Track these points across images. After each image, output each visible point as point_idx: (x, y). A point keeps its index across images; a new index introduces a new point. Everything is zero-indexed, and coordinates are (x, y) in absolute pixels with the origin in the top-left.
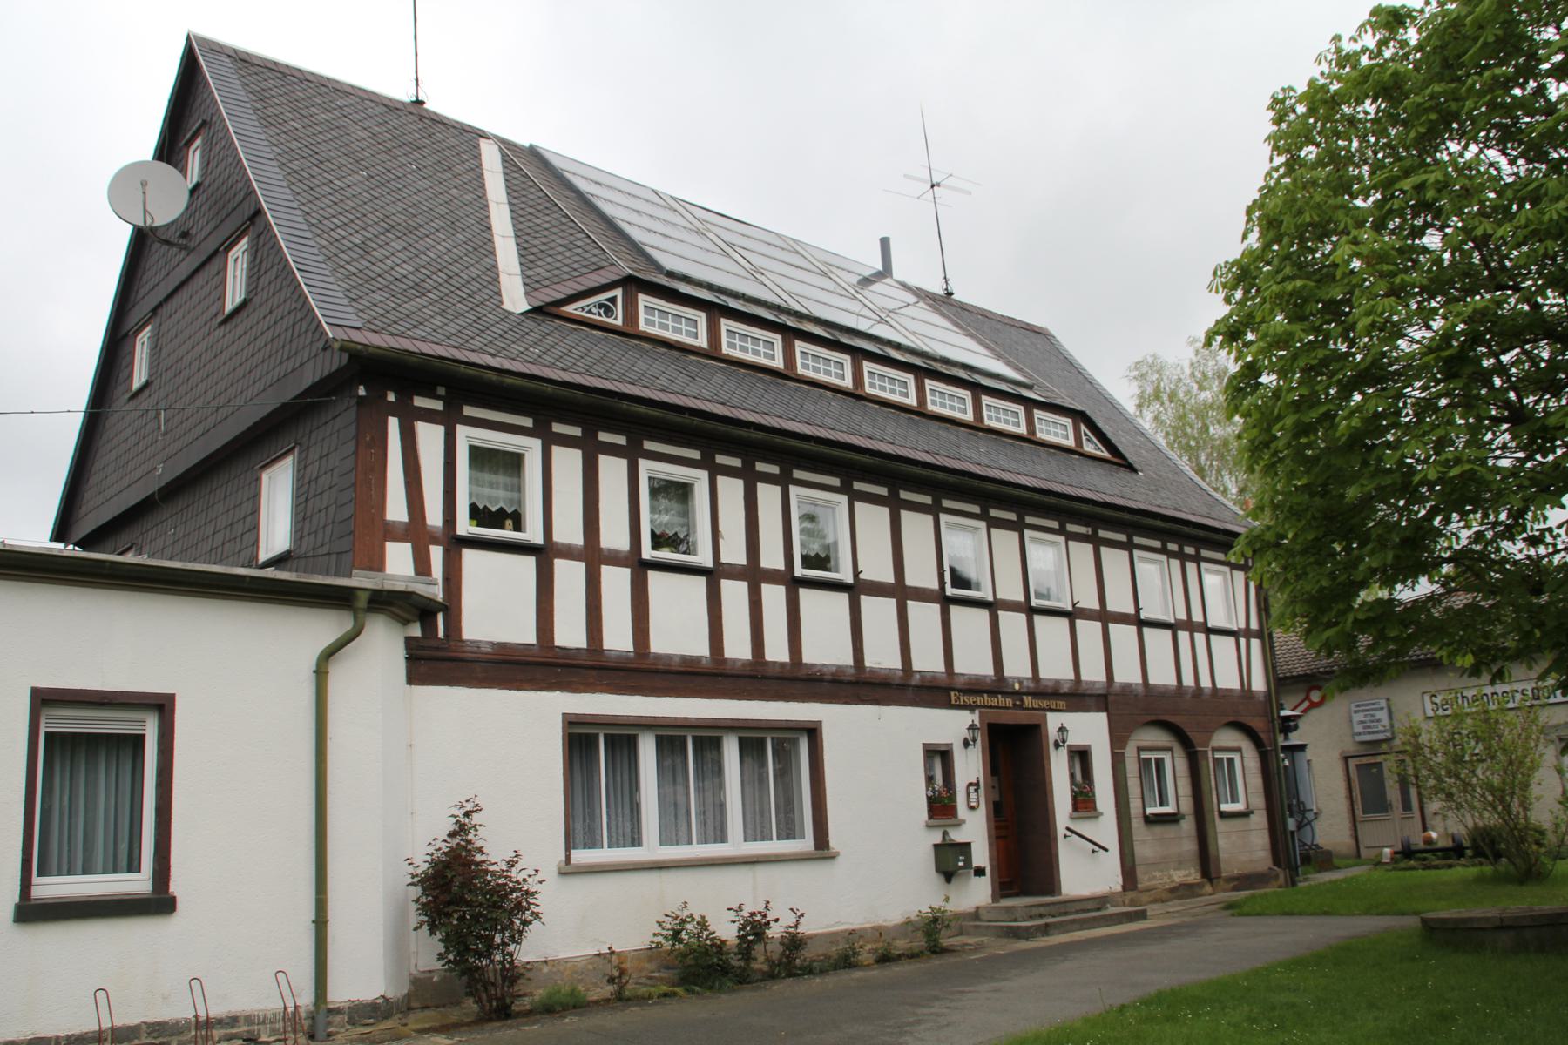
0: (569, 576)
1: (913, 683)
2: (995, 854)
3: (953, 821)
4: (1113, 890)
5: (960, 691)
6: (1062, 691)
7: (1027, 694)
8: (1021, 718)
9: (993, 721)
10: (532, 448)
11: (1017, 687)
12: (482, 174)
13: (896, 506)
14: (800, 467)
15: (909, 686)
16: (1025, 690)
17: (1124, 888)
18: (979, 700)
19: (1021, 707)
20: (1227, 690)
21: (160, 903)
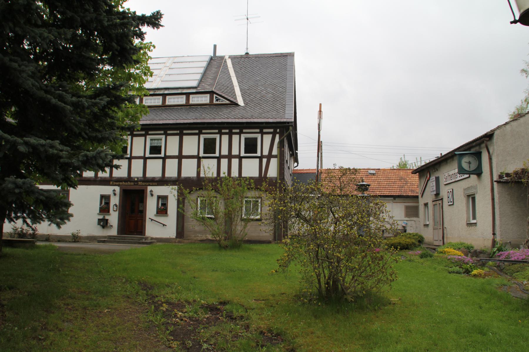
0: (224, 162)
1: (98, 180)
3: (108, 214)
4: (171, 237)
5: (114, 181)
6: (155, 180)
7: (140, 181)
8: (137, 188)
9: (125, 189)
11: (136, 179)
12: (231, 79)
13: (181, 136)
14: (204, 130)
15: (97, 181)
16: (139, 180)
17: (177, 237)
18: (121, 183)
19: (137, 185)
20: (169, 177)
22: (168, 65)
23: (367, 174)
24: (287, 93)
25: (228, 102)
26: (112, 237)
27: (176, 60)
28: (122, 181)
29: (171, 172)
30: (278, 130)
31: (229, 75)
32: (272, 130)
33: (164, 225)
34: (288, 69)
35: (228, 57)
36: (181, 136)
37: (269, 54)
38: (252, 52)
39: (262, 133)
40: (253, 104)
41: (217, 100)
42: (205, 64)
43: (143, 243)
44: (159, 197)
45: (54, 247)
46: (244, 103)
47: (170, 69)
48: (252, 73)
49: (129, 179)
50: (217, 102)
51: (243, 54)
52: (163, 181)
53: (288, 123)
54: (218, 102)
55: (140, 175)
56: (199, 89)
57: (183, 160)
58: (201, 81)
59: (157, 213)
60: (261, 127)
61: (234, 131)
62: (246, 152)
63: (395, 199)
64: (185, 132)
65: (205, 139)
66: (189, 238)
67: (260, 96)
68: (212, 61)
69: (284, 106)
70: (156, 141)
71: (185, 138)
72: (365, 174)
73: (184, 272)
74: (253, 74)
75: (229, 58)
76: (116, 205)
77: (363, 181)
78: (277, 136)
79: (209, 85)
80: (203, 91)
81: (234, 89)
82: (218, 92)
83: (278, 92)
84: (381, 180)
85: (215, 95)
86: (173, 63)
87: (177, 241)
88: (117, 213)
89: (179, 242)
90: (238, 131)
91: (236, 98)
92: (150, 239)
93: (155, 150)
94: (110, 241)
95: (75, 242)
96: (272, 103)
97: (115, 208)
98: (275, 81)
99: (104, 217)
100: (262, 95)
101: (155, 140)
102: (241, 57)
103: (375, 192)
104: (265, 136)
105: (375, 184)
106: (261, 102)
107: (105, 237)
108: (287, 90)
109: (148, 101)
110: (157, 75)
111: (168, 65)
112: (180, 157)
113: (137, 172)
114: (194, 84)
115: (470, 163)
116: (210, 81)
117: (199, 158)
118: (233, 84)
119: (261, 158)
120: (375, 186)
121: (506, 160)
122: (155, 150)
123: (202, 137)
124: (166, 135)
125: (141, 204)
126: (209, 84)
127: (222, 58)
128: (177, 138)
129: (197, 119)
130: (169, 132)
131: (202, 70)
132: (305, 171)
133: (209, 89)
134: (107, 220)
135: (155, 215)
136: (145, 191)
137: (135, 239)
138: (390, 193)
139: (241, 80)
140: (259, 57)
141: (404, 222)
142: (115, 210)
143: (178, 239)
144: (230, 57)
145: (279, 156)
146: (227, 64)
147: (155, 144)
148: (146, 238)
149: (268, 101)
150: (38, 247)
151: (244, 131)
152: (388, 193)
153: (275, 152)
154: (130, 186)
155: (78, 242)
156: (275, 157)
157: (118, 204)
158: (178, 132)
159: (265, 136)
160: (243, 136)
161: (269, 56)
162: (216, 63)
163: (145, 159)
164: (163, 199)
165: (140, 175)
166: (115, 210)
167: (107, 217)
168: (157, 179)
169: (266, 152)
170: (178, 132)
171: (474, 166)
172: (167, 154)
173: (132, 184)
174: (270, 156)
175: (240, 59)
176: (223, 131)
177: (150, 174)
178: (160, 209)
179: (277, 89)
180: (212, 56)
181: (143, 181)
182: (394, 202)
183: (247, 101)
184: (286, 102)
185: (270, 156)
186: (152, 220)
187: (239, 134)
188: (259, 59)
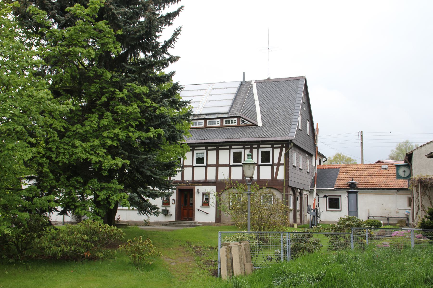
2: (177, 212)
4: (212, 222)
7: (190, 183)
8: (188, 187)
10: (271, 150)
11: (187, 182)
13: (217, 150)
17: (216, 222)
19: (188, 185)
21: (341, 211)
22: (208, 91)
23: (380, 169)
24: (294, 115)
25: (250, 124)
26: (171, 222)
27: (215, 86)
28: (177, 183)
29: (211, 176)
30: (284, 145)
31: (254, 99)
32: (280, 145)
33: (207, 213)
34: (298, 93)
35: (254, 81)
36: (217, 150)
37: (286, 78)
38: (272, 77)
39: (273, 148)
40: (268, 125)
41: (243, 122)
42: (235, 90)
43: (193, 226)
44: (203, 194)
45: (138, 228)
46: (262, 124)
47: (209, 95)
48: (271, 96)
49: (182, 181)
50: (243, 124)
51: (266, 78)
52: (206, 183)
53: (291, 140)
54: (244, 124)
55: (190, 178)
56: (230, 114)
57: (219, 168)
58: (232, 107)
59: (202, 205)
60: (273, 143)
61: (254, 146)
62: (262, 161)
63: (399, 191)
64: (220, 147)
65: (234, 153)
66: (224, 222)
67: (274, 118)
68: (241, 87)
69: (290, 126)
70: (200, 154)
71: (220, 151)
72: (378, 169)
73: (209, 238)
74: (272, 97)
75: (255, 83)
76: (174, 200)
77: (352, 180)
78: (284, 149)
79: (237, 110)
80: (232, 116)
81: (256, 112)
82: (243, 117)
83: (288, 114)
84: (391, 175)
85: (241, 119)
86: (213, 89)
87: (216, 225)
88: (174, 206)
89: (217, 225)
90: (256, 146)
91: (256, 121)
92: (197, 223)
93: (200, 160)
94: (170, 225)
95: (146, 226)
96: (282, 123)
97: (173, 202)
98: (287, 104)
99: (166, 208)
100: (276, 117)
101: (199, 153)
102: (264, 81)
103: (381, 186)
104: (275, 150)
105: (384, 178)
106: (275, 123)
107: (167, 222)
108: (295, 112)
109: (195, 124)
110: (200, 102)
111: (208, 92)
112: (217, 166)
113: (188, 177)
114: (226, 110)
115: (404, 171)
116: (238, 106)
117: (230, 166)
118: (255, 107)
119: (272, 166)
120: (383, 180)
121: (421, 171)
122: (200, 160)
123: (232, 151)
124: (207, 150)
125: (191, 199)
126: (237, 109)
127: (249, 83)
128: (215, 152)
129: (227, 138)
130: (209, 148)
131: (232, 97)
132: (327, 167)
133: (237, 114)
134: (168, 210)
135: (201, 207)
136: (194, 190)
137: (187, 223)
138: (394, 186)
139: (262, 104)
140: (277, 81)
141: (406, 211)
142: (173, 203)
143: (217, 224)
144: (256, 82)
145: (285, 164)
146: (252, 89)
147: (200, 156)
148: (195, 223)
149: (279, 122)
150: (130, 228)
151: (261, 146)
152: (392, 186)
153: (282, 161)
154: (184, 187)
155: (149, 226)
156: (282, 164)
157: (175, 199)
158: (215, 148)
159: (275, 150)
160: (260, 150)
161: (286, 80)
162: (244, 88)
163: (193, 167)
164: (206, 195)
165: (190, 178)
166: (173, 203)
167: (168, 209)
168: (202, 181)
169: (276, 162)
170: (215, 148)
171: (407, 174)
172: (208, 164)
173: (185, 185)
174: (279, 164)
175: (263, 83)
176: (246, 147)
177: (196, 178)
178: (204, 202)
179: (287, 111)
180: (242, 81)
181: (192, 183)
182: (398, 194)
183: (265, 122)
184: (293, 122)
185: (279, 164)
186: (199, 210)
187: (257, 148)
188: (277, 83)
